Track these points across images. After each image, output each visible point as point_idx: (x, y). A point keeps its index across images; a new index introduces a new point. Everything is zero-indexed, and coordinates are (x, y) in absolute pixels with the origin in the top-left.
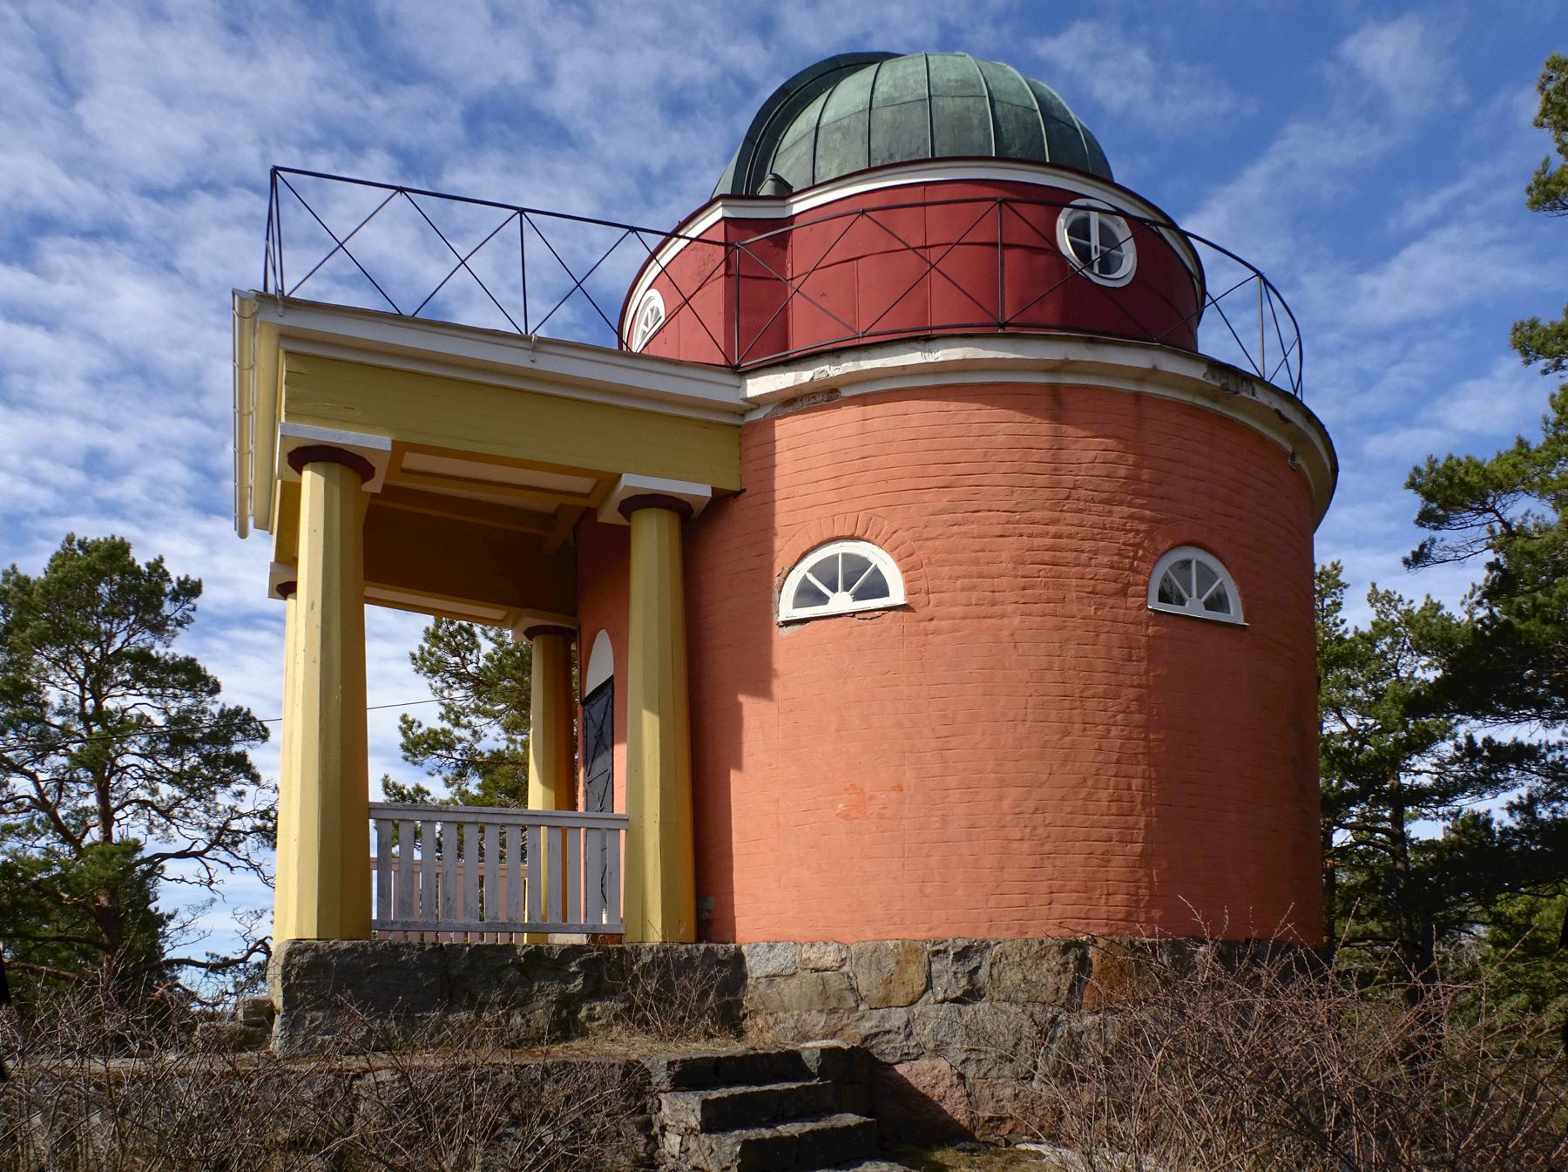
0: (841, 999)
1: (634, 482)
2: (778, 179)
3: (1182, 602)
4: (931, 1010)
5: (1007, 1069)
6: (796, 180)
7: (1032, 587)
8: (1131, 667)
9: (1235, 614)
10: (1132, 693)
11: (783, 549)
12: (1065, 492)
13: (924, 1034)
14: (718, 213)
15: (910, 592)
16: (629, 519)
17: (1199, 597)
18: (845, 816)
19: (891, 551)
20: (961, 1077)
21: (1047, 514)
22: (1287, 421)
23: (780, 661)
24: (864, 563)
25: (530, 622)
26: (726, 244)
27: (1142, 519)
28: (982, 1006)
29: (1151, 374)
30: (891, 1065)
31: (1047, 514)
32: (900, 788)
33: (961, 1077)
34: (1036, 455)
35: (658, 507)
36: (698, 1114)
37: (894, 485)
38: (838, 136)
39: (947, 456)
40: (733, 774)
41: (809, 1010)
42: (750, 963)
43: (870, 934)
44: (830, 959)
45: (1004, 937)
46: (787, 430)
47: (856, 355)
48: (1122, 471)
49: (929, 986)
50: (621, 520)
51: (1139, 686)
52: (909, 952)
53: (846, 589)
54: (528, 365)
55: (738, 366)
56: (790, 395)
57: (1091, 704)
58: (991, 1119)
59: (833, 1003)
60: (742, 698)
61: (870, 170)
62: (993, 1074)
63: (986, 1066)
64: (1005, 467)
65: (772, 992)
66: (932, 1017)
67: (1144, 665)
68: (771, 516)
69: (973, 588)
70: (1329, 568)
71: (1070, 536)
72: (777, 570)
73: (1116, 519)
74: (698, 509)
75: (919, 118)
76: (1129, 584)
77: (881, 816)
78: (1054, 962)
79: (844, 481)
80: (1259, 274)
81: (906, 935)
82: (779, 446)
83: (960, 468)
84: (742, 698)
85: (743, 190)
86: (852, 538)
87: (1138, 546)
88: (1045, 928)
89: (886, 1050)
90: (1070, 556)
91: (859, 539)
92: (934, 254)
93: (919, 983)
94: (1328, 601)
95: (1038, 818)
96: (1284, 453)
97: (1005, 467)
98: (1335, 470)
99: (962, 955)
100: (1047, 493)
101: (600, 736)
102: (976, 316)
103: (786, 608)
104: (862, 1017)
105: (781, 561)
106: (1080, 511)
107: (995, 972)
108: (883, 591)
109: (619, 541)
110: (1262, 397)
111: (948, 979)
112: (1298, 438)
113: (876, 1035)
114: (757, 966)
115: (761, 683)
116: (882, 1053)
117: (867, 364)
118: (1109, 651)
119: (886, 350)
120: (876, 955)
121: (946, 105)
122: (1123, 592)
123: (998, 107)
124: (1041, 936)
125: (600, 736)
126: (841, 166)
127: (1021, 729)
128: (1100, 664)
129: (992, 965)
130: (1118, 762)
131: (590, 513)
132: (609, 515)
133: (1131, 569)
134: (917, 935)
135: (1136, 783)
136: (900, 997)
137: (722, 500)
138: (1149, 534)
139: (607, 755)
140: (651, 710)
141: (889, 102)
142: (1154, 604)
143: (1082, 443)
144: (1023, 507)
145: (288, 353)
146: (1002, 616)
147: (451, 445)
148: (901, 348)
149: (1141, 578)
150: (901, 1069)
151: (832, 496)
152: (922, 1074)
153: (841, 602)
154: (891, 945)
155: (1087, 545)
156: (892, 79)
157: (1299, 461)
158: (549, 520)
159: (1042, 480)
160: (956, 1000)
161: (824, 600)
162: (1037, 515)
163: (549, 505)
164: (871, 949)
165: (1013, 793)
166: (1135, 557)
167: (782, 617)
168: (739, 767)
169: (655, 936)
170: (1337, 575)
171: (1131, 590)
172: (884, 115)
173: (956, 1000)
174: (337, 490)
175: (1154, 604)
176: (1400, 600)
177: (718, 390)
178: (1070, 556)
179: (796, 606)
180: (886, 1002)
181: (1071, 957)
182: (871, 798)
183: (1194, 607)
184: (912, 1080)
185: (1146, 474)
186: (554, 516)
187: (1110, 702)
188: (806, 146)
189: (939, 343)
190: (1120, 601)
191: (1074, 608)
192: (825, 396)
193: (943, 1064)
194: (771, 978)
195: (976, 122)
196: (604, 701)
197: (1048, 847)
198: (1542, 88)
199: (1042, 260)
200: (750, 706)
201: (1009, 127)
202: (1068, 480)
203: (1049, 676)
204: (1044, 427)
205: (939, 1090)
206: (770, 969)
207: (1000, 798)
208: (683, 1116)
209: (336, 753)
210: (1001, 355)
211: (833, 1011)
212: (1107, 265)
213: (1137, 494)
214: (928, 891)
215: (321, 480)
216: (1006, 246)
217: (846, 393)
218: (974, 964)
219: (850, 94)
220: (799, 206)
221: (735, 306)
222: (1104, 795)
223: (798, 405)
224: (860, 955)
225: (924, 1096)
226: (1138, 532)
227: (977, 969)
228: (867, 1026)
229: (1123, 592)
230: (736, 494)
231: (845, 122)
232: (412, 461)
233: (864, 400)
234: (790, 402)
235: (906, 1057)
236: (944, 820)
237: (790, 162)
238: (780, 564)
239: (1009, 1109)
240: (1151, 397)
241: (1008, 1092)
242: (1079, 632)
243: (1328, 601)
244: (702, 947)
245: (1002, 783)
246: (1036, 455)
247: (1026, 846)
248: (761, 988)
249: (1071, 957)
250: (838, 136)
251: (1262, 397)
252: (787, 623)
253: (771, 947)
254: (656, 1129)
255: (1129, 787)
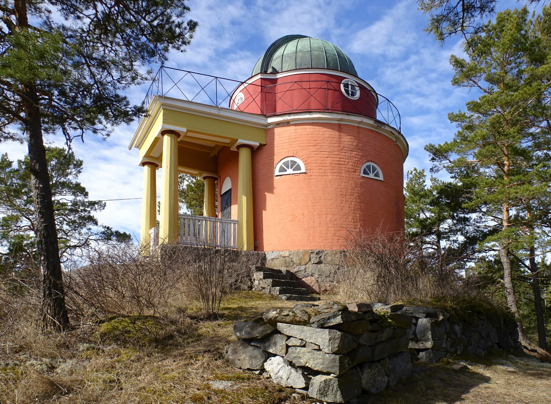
0: (289, 264)
1: (241, 141)
2: (273, 68)
3: (369, 175)
4: (311, 265)
5: (328, 279)
6: (278, 68)
7: (334, 169)
8: (357, 189)
9: (381, 178)
10: (356, 195)
11: (276, 158)
12: (342, 148)
13: (309, 271)
14: (259, 76)
15: (306, 170)
16: (238, 150)
17: (373, 173)
18: (291, 221)
19: (302, 160)
20: (317, 281)
21: (338, 153)
22: (393, 134)
23: (276, 184)
24: (295, 162)
25: (205, 175)
26: (261, 86)
27: (359, 155)
28: (323, 265)
29: (361, 122)
30: (301, 279)
31: (338, 153)
32: (303, 215)
33: (317, 281)
34: (335, 139)
35: (246, 147)
36: (263, 275)
37: (303, 145)
38: (288, 58)
39: (315, 139)
40: (264, 212)
41: (282, 267)
42: (267, 256)
43: (296, 249)
44: (287, 255)
45: (328, 250)
46: (277, 130)
47: (294, 115)
48: (355, 144)
49: (310, 260)
50: (236, 150)
51: (358, 193)
52: (305, 252)
53: (291, 168)
54: (217, 113)
55: (265, 115)
56: (278, 123)
57: (348, 197)
58: (324, 291)
59: (288, 265)
60: (266, 193)
61: (296, 69)
62: (325, 280)
63: (323, 278)
64: (328, 142)
65: (273, 263)
66: (311, 268)
67: (360, 188)
68: (274, 151)
69: (321, 169)
70: (421, 171)
71: (343, 158)
72: (275, 163)
73: (353, 155)
74: (255, 148)
75: (308, 56)
76: (356, 170)
77: (299, 221)
78: (338, 255)
79: (291, 143)
80: (387, 99)
81: (305, 249)
82: (275, 134)
83: (318, 142)
84: (266, 193)
85: (264, 71)
86: (293, 156)
87: (358, 161)
88: (337, 248)
89: (300, 275)
90: (343, 163)
91: (294, 157)
92: (312, 91)
93: (308, 260)
94: (421, 180)
95: (335, 222)
96: (394, 141)
97: (328, 142)
98: (408, 145)
99: (317, 253)
100: (338, 148)
101: (227, 204)
102: (321, 107)
103: (277, 172)
104: (294, 268)
105: (276, 161)
106: (345, 153)
107: (325, 257)
108: (300, 169)
109: (235, 156)
110: (387, 128)
111: (314, 259)
112: (397, 138)
113: (298, 272)
114: (269, 257)
115: (271, 190)
116: (299, 276)
117: (297, 117)
118: (351, 185)
119: (300, 114)
120: (298, 253)
121: (315, 53)
122: (355, 172)
123: (327, 54)
124: (336, 249)
125: (227, 204)
126: (289, 66)
127: (331, 202)
128: (349, 188)
129: (325, 256)
130: (354, 210)
131: (229, 148)
132: (234, 148)
133: (357, 166)
134: (307, 249)
135: (358, 215)
136: (303, 263)
137: (261, 146)
138: (361, 158)
139: (229, 208)
140: (245, 195)
141: (301, 51)
142: (362, 174)
143: (346, 137)
144: (332, 151)
145: (163, 109)
146: (327, 176)
147: (196, 130)
148: (304, 114)
149: (359, 168)
150: (303, 279)
151: (288, 147)
152: (308, 280)
153: (290, 171)
154: (301, 251)
155: (347, 160)
156: (303, 44)
157: (397, 143)
158: (212, 149)
159: (336, 145)
160: (316, 264)
161: (286, 171)
162: (335, 153)
163: (212, 145)
164: (297, 251)
165: (329, 216)
166: (358, 164)
167: (276, 174)
168: (265, 210)
169: (245, 248)
170: (423, 173)
171: (357, 171)
172: (300, 54)
173: (316, 264)
174: (173, 141)
175: (362, 174)
176: (438, 180)
177: (261, 120)
178: (343, 163)
179: (280, 171)
180: (300, 264)
181: (342, 254)
182: (297, 217)
183: (372, 176)
184: (306, 282)
185: (360, 145)
186: (214, 148)
187: (352, 197)
188: (280, 59)
189: (313, 113)
190: (354, 174)
191: (343, 175)
192: (287, 124)
193: (313, 278)
194: (272, 259)
195: (322, 58)
196: (228, 194)
197: (337, 229)
198: (450, 61)
199: (337, 93)
200: (268, 196)
201: (330, 59)
202: (342, 145)
203: (338, 190)
204: (337, 133)
205: (312, 284)
206: (272, 257)
207: (327, 217)
208: (259, 277)
209: (173, 201)
210: (327, 117)
211: (287, 267)
212: (353, 94)
213: (358, 149)
214: (310, 238)
215: (169, 138)
216: (328, 89)
217: (291, 123)
218: (320, 255)
219: (291, 47)
220: (279, 76)
221: (264, 100)
222: (350, 218)
223: (280, 125)
224: (294, 253)
225: (309, 285)
226: (358, 158)
227: (321, 256)
228: (295, 270)
229: (355, 172)
230: (265, 145)
231: (290, 55)
232: (189, 134)
233: (295, 125)
234: (278, 124)
235: (305, 277)
236: (314, 222)
237: (275, 63)
238: (276, 162)
239: (328, 288)
240: (361, 128)
241: (328, 285)
242: (345, 180)
243: (421, 180)
244: (256, 252)
245: (327, 214)
246: (335, 139)
247: (332, 229)
248: (270, 262)
249: (342, 254)
250: (288, 58)
251: (387, 128)
252: (277, 176)
253: (273, 252)
254: (253, 280)
255: (356, 216)
